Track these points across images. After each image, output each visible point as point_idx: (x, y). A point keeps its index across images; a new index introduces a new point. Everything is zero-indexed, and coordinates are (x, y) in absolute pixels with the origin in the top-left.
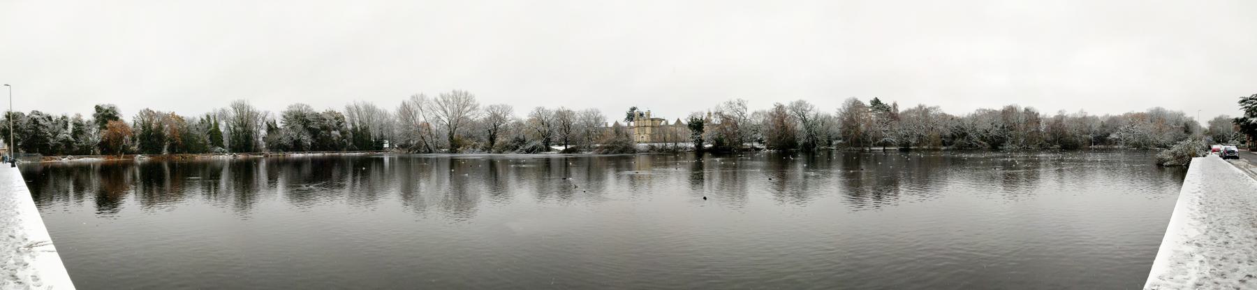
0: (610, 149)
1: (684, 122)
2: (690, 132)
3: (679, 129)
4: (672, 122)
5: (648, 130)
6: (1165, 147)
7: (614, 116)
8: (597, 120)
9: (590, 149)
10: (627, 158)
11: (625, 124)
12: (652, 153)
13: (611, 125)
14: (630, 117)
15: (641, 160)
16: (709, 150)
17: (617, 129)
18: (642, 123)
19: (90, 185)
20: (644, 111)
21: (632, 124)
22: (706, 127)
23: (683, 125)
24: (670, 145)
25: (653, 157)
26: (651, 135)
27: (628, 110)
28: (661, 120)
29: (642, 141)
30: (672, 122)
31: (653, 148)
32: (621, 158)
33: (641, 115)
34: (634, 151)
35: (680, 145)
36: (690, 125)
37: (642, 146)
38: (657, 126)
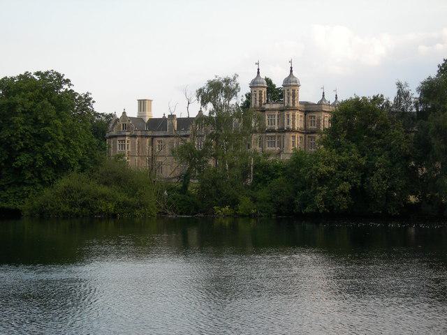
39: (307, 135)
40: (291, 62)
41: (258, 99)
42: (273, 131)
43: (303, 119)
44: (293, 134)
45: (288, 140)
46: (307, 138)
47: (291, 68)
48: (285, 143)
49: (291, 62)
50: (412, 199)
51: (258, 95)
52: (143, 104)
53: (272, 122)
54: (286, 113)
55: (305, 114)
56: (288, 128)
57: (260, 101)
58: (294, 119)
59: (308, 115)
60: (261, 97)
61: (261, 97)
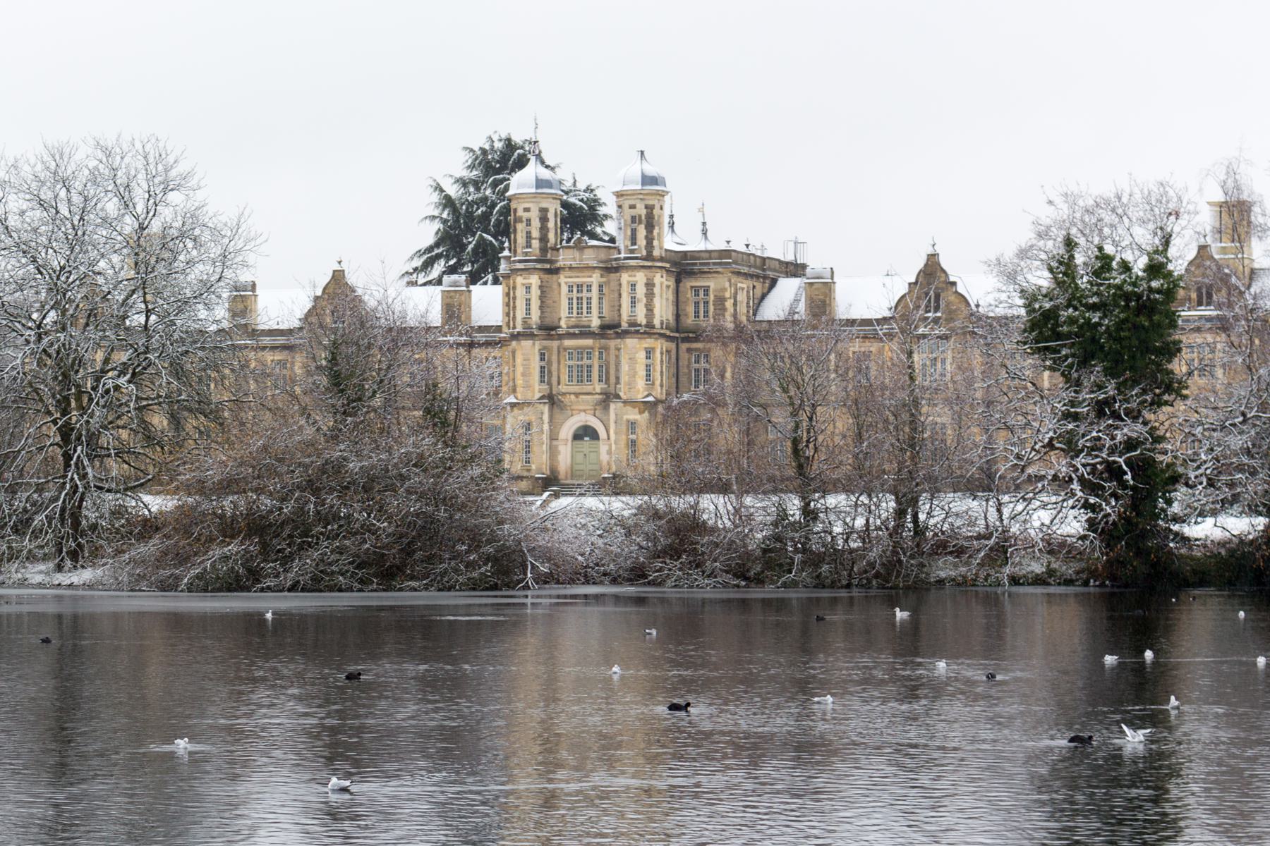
0: (269, 543)
1: (985, 290)
2: (1043, 394)
3: (939, 363)
4: (867, 294)
5: (640, 368)
6: (1008, 427)
7: (314, 223)
8: (151, 256)
9: (75, 542)
10: (426, 635)
11: (423, 304)
12: (680, 585)
13: (282, 304)
14: (472, 234)
15: (575, 676)
16: (1238, 571)
17: (345, 339)
18: (578, 293)
19: (628, 669)
20: (602, 173)
21: (487, 303)
22: (1199, 349)
23: (977, 327)
24: (847, 515)
25: (685, 626)
26: (672, 418)
27: (452, 168)
28: (765, 272)
29: (576, 464)
30: (867, 294)
31: (683, 539)
32: (368, 632)
33: (579, 218)
34: (505, 568)
35: (953, 511)
36: (1044, 328)
37: (579, 519)
38: (731, 328)
39: (684, 346)
40: (701, 210)
41: (536, 234)
42: (585, 333)
43: (671, 297)
44: (649, 342)
45: (632, 360)
46: (684, 356)
47: (704, 224)
48: (625, 367)
49: (701, 210)
50: (900, 615)
51: (536, 223)
52: (1236, 216)
53: (580, 304)
54: (625, 277)
55: (678, 282)
56: (633, 324)
57: (543, 239)
58: (650, 295)
59: (689, 283)
60: (544, 229)
61: (544, 229)
